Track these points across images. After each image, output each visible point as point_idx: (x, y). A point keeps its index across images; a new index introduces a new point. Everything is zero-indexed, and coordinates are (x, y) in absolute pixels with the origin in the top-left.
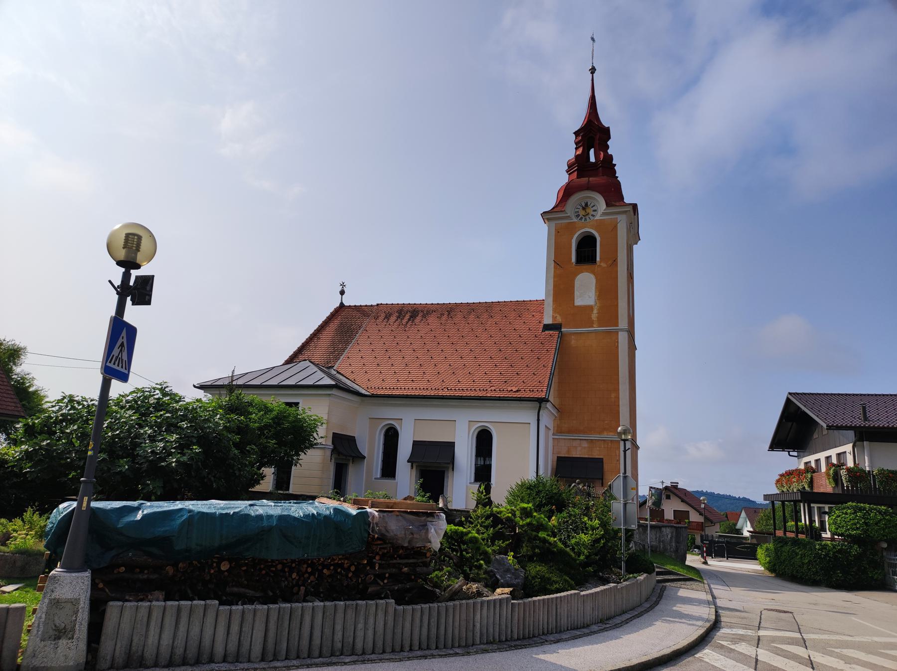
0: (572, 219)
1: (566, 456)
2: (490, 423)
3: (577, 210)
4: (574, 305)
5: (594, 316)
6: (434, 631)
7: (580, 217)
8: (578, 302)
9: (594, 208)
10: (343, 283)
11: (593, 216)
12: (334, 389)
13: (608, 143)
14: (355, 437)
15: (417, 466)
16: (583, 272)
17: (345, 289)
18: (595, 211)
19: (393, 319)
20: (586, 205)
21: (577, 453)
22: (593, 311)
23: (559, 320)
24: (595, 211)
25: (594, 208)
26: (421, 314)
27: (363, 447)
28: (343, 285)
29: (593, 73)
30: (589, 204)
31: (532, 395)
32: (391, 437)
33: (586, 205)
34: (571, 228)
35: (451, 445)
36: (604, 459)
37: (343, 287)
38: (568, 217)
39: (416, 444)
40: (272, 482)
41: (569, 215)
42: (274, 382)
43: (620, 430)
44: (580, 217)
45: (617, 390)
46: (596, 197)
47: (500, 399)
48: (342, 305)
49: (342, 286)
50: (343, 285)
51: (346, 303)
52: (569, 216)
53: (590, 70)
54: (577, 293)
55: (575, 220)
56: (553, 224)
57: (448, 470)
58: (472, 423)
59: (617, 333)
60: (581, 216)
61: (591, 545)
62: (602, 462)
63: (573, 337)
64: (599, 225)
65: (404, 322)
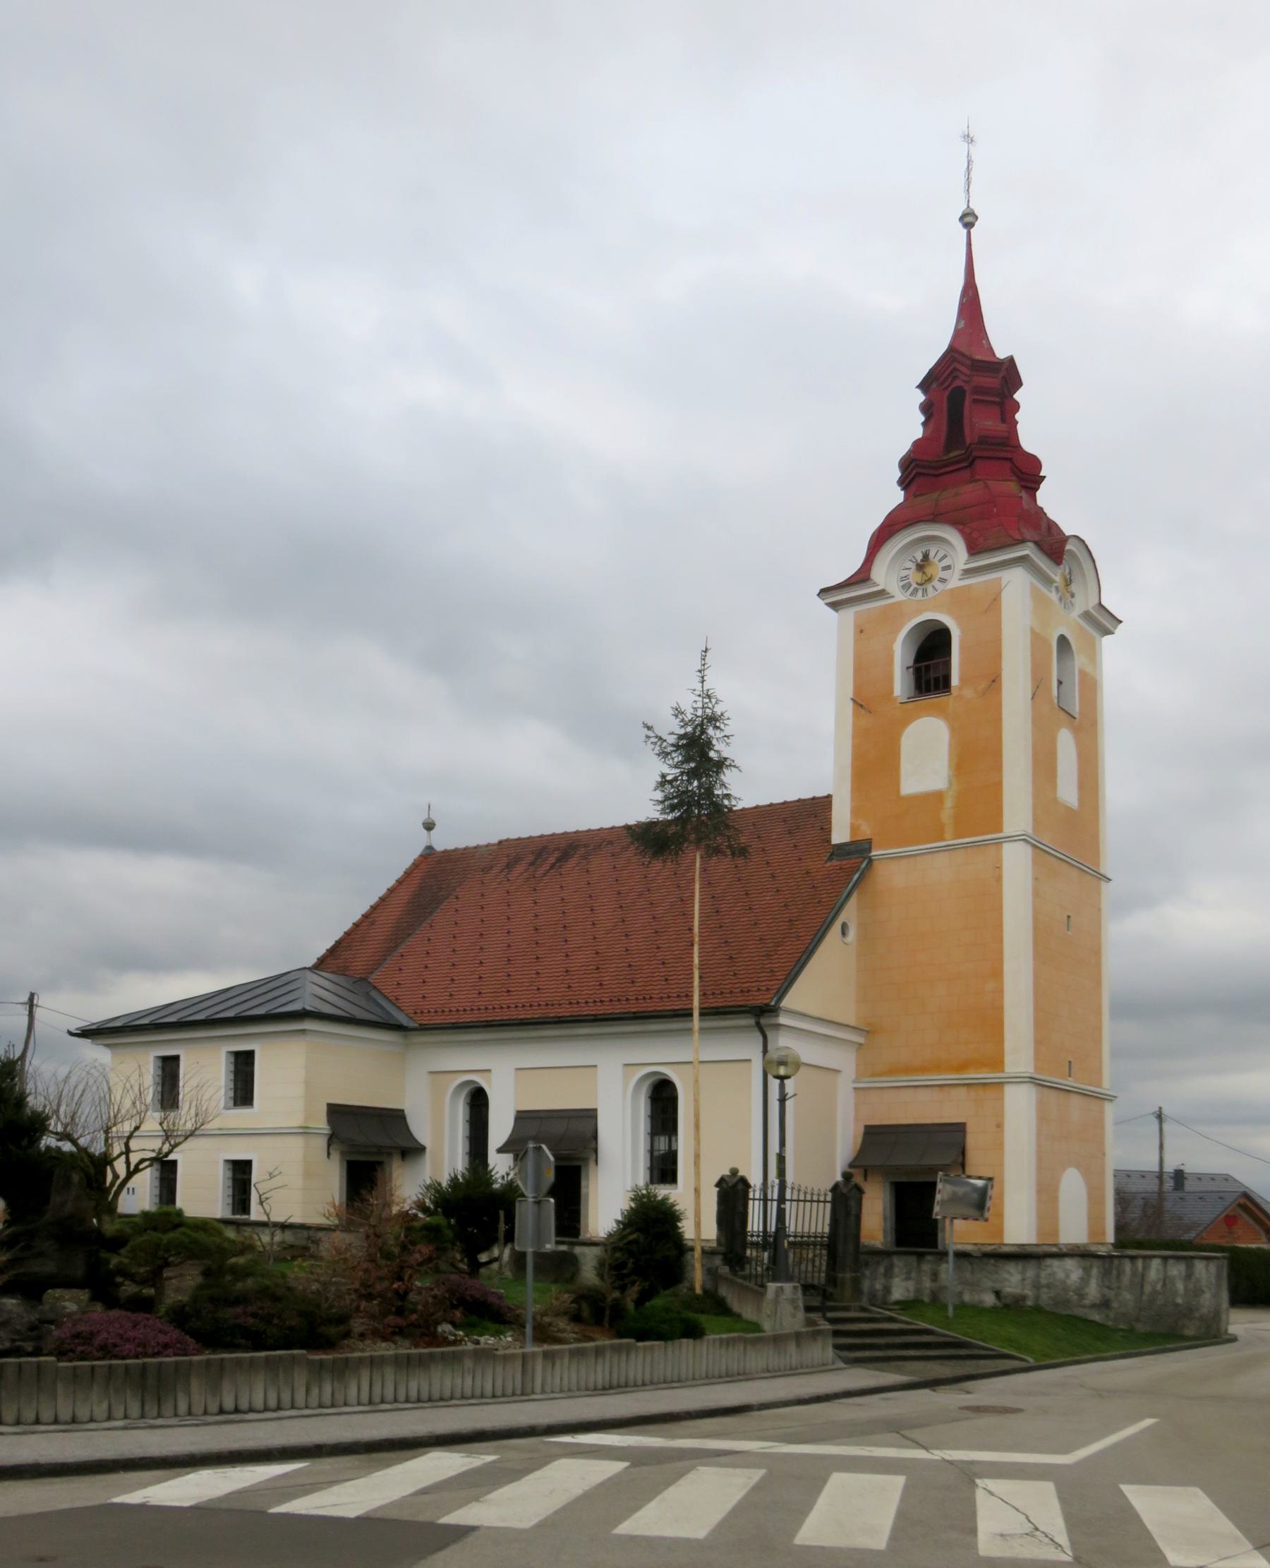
2: (672, 1066)
3: (905, 573)
11: (943, 580)
14: (403, 1111)
16: (918, 717)
18: (947, 568)
19: (519, 869)
20: (926, 557)
24: (947, 568)
26: (582, 851)
27: (421, 1129)
29: (969, 226)
31: (740, 1000)
32: (478, 1101)
34: (893, 616)
35: (590, 1116)
36: (969, 1129)
39: (523, 1118)
40: (220, 1199)
42: (261, 1011)
56: (849, 614)
57: (587, 1165)
60: (914, 586)
61: (167, 1264)
62: (596, 1117)
64: (957, 599)
65: (540, 872)
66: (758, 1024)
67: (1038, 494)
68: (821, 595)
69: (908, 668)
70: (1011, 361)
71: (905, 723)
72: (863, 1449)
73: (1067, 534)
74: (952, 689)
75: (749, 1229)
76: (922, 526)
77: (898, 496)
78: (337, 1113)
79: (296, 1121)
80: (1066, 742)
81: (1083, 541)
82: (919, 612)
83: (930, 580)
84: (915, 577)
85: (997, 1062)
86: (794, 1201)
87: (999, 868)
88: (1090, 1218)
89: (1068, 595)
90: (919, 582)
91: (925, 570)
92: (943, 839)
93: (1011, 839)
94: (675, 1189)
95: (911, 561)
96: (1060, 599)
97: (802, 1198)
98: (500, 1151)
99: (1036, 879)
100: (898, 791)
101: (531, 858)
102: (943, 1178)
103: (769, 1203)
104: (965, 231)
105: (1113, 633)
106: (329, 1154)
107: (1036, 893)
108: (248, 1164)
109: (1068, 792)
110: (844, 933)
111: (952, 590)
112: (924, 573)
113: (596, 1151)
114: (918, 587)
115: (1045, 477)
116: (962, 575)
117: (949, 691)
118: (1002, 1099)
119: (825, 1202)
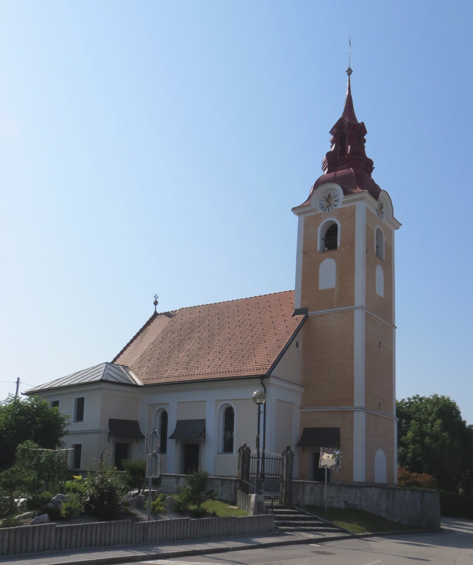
0: (318, 211)
7: (324, 208)
8: (322, 286)
9: (336, 199)
10: (156, 295)
13: (365, 137)
17: (158, 300)
18: (337, 201)
20: (329, 195)
24: (337, 201)
25: (336, 199)
27: (145, 430)
28: (156, 297)
30: (332, 195)
32: (164, 416)
33: (329, 195)
34: (317, 219)
35: (203, 422)
37: (156, 299)
38: (314, 210)
41: (314, 208)
43: (255, 395)
44: (324, 208)
46: (335, 188)
47: (233, 379)
48: (156, 315)
49: (155, 298)
50: (156, 297)
51: (159, 312)
52: (314, 209)
53: (346, 71)
55: (320, 211)
66: (262, 383)
67: (372, 174)
68: (292, 210)
69: (322, 239)
70: (363, 123)
71: (320, 261)
73: (382, 189)
74: (338, 248)
75: (251, 470)
80: (379, 271)
81: (387, 193)
83: (331, 205)
84: (325, 204)
85: (351, 401)
87: (353, 320)
89: (381, 213)
90: (327, 206)
91: (329, 201)
92: (333, 308)
94: (232, 454)
95: (324, 198)
96: (378, 214)
98: (171, 438)
100: (318, 288)
102: (323, 450)
103: (266, 460)
104: (348, 76)
105: (399, 229)
106: (109, 440)
107: (367, 331)
109: (380, 291)
110: (297, 346)
111: (338, 209)
112: (329, 202)
113: (204, 437)
114: (326, 208)
115: (374, 168)
116: (342, 203)
117: (337, 249)
118: (353, 418)
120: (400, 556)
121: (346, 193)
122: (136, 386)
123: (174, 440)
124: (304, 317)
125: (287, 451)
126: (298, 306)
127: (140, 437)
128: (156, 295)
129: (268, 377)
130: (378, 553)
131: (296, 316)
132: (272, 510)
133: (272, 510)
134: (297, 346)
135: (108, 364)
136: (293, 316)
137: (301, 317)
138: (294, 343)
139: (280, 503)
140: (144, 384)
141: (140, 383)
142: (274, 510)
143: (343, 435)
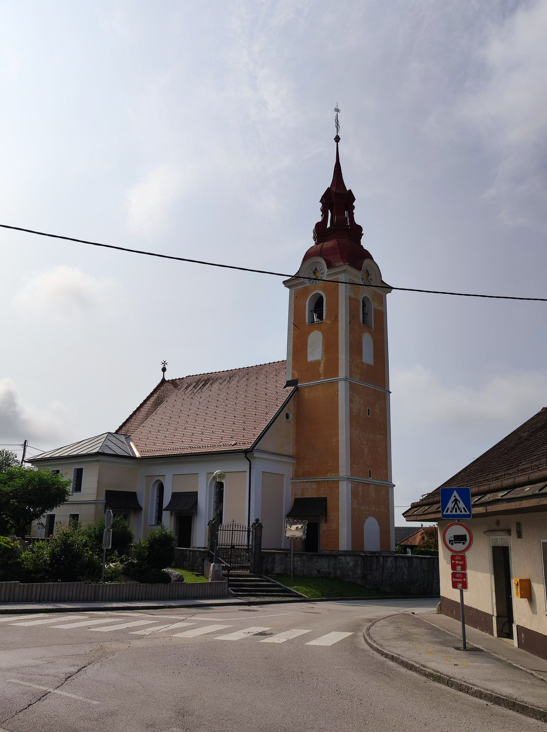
1: (301, 497)
4: (307, 361)
5: (321, 369)
6: (38, 595)
9: (321, 272)
10: (165, 362)
12: (99, 456)
15: (175, 514)
17: (166, 366)
19: (190, 389)
20: (316, 269)
21: (308, 495)
22: (320, 365)
23: (297, 376)
27: (142, 502)
28: (164, 363)
30: (318, 269)
32: (161, 488)
33: (316, 269)
34: (305, 292)
35: (195, 494)
37: (164, 365)
39: (174, 495)
45: (337, 435)
48: (163, 381)
50: (164, 363)
51: (167, 379)
54: (309, 350)
58: (209, 474)
59: (337, 382)
62: (326, 501)
63: (306, 390)
66: (246, 457)
71: (309, 333)
72: (435, 671)
76: (314, 258)
77: (312, 243)
78: (109, 494)
79: (93, 498)
82: (314, 290)
86: (238, 531)
88: (381, 540)
93: (341, 380)
97: (241, 529)
99: (351, 395)
101: (195, 384)
108: (77, 516)
109: (368, 357)
110: (287, 416)
115: (363, 234)
119: (245, 531)
120: (227, 612)
121: (330, 265)
122: (134, 458)
123: (168, 513)
124: (294, 388)
125: (256, 523)
126: (290, 378)
127: (138, 509)
128: (165, 362)
129: (251, 451)
130: (227, 612)
131: (287, 388)
132: (228, 578)
133: (228, 578)
134: (287, 416)
135: (110, 435)
136: (285, 387)
137: (292, 388)
138: (283, 414)
139: (250, 573)
140: (142, 457)
141: (138, 455)
142: (229, 578)
143: (330, 504)
